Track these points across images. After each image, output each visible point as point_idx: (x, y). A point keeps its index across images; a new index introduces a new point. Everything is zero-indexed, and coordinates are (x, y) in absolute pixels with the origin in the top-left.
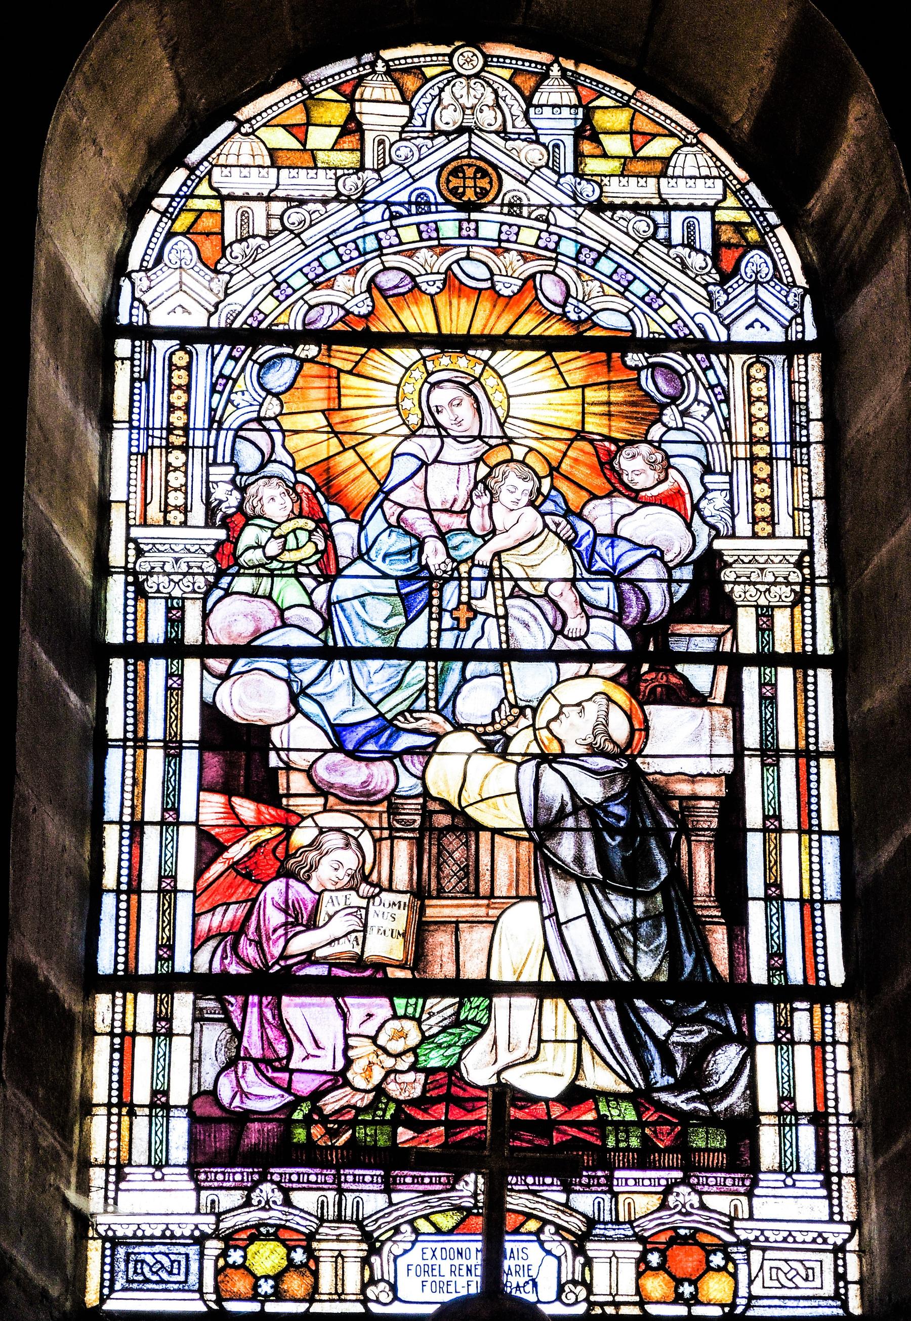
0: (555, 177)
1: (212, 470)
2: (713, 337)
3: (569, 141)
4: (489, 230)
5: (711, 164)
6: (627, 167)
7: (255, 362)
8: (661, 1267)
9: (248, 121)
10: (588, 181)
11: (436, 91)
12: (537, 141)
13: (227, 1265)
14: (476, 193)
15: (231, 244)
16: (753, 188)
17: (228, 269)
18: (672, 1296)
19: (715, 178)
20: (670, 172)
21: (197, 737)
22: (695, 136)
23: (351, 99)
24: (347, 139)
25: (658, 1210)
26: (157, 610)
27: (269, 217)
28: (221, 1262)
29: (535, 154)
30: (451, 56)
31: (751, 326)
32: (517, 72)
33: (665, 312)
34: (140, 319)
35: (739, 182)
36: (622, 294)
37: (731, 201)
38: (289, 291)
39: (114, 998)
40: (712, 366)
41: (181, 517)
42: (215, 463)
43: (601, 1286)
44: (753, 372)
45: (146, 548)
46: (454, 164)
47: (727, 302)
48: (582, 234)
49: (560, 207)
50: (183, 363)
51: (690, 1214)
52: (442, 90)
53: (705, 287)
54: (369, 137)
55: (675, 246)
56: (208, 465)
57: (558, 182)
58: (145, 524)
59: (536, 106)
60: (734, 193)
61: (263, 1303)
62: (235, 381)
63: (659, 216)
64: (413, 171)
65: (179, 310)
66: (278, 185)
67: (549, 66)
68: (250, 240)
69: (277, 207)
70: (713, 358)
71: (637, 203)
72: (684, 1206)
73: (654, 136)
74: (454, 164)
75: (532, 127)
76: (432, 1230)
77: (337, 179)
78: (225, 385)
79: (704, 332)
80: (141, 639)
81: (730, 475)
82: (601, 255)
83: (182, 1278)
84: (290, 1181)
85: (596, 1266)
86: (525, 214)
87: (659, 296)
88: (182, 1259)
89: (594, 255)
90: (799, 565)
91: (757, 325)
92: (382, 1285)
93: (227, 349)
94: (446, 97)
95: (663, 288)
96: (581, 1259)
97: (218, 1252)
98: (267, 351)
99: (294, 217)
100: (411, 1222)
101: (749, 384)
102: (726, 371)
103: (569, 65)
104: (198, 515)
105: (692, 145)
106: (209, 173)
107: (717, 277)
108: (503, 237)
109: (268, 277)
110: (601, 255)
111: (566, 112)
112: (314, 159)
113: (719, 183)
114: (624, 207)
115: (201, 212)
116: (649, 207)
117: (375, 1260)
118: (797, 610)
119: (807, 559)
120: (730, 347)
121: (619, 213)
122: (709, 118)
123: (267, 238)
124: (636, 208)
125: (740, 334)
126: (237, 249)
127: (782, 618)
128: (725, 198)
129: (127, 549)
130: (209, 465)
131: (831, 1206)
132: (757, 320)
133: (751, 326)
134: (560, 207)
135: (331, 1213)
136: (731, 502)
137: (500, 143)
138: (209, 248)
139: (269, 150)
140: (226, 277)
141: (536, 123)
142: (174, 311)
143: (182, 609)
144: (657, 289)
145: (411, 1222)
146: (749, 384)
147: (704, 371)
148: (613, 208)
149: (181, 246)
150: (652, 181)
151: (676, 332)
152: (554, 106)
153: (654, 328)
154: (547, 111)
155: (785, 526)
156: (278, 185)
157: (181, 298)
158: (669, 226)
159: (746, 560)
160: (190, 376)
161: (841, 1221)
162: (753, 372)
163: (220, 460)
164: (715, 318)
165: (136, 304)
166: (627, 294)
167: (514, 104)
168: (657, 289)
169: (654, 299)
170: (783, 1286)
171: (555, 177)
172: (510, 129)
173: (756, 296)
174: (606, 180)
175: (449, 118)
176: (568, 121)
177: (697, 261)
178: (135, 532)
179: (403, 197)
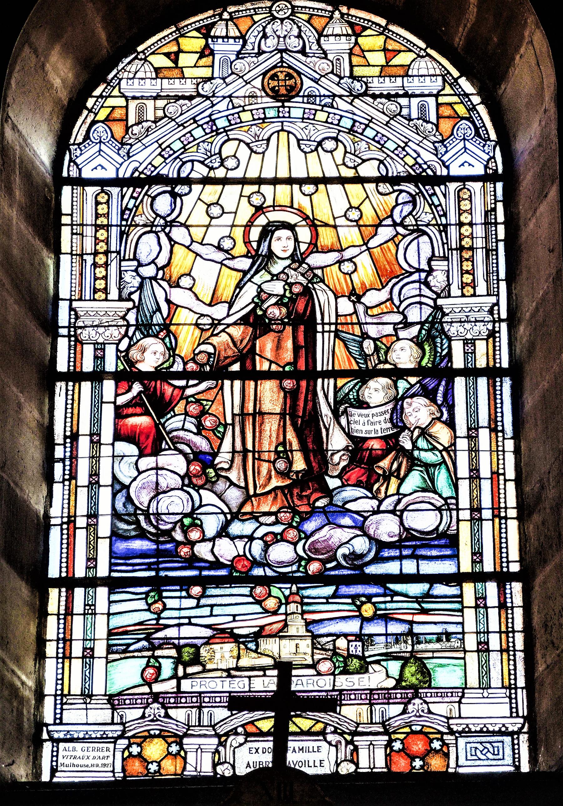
0: (337, 79)
1: (123, 263)
3: (346, 57)
4: (297, 113)
5: (436, 66)
6: (385, 71)
7: (149, 196)
9: (143, 52)
10: (358, 81)
11: (261, 28)
12: (326, 58)
14: (286, 90)
15: (132, 126)
16: (463, 82)
17: (129, 142)
20: (410, 73)
21: (56, 464)
22: (425, 50)
23: (206, 36)
24: (204, 60)
26: (88, 350)
27: (155, 109)
28: (126, 754)
29: (324, 66)
30: (270, 8)
34: (74, 173)
35: (453, 78)
37: (448, 90)
38: (171, 152)
39: (60, 592)
40: (435, 194)
42: (124, 260)
43: (364, 763)
45: (82, 314)
46: (272, 72)
47: (446, 152)
48: (354, 114)
49: (340, 97)
50: (104, 200)
52: (264, 28)
53: (434, 143)
54: (217, 57)
55: (413, 120)
57: (339, 82)
60: (450, 85)
63: (404, 101)
64: (246, 78)
65: (99, 168)
67: (333, 12)
68: (144, 124)
69: (161, 103)
70: (436, 188)
71: (389, 94)
72: (418, 711)
73: (400, 51)
74: (272, 72)
75: (322, 49)
80: (78, 370)
84: (170, 703)
86: (318, 102)
87: (403, 149)
89: (363, 126)
90: (491, 312)
91: (466, 164)
92: (226, 765)
95: (406, 144)
97: (124, 746)
99: (172, 109)
101: (459, 202)
103: (344, 9)
104: (114, 294)
105: (423, 57)
109: (156, 145)
110: (367, 126)
112: (182, 72)
113: (440, 79)
114: (381, 96)
115: (114, 108)
116: (397, 95)
118: (491, 340)
119: (496, 308)
121: (378, 100)
122: (437, 40)
123: (155, 122)
124: (388, 97)
125: (455, 171)
126: (136, 129)
127: (481, 346)
128: (443, 89)
129: (70, 315)
131: (511, 708)
134: (340, 97)
136: (448, 277)
137: (303, 58)
138: (119, 130)
139: (154, 68)
141: (325, 47)
142: (96, 168)
143: (104, 350)
144: (403, 145)
146: (459, 202)
147: (430, 196)
148: (374, 97)
149: (101, 129)
150: (399, 80)
151: (414, 171)
152: (336, 35)
153: (401, 169)
155: (482, 288)
157: (100, 160)
158: (409, 107)
161: (518, 716)
163: (127, 257)
167: (310, 35)
168: (403, 145)
170: (480, 759)
172: (308, 50)
173: (465, 147)
174: (370, 80)
176: (344, 44)
178: (75, 304)
179: (241, 93)
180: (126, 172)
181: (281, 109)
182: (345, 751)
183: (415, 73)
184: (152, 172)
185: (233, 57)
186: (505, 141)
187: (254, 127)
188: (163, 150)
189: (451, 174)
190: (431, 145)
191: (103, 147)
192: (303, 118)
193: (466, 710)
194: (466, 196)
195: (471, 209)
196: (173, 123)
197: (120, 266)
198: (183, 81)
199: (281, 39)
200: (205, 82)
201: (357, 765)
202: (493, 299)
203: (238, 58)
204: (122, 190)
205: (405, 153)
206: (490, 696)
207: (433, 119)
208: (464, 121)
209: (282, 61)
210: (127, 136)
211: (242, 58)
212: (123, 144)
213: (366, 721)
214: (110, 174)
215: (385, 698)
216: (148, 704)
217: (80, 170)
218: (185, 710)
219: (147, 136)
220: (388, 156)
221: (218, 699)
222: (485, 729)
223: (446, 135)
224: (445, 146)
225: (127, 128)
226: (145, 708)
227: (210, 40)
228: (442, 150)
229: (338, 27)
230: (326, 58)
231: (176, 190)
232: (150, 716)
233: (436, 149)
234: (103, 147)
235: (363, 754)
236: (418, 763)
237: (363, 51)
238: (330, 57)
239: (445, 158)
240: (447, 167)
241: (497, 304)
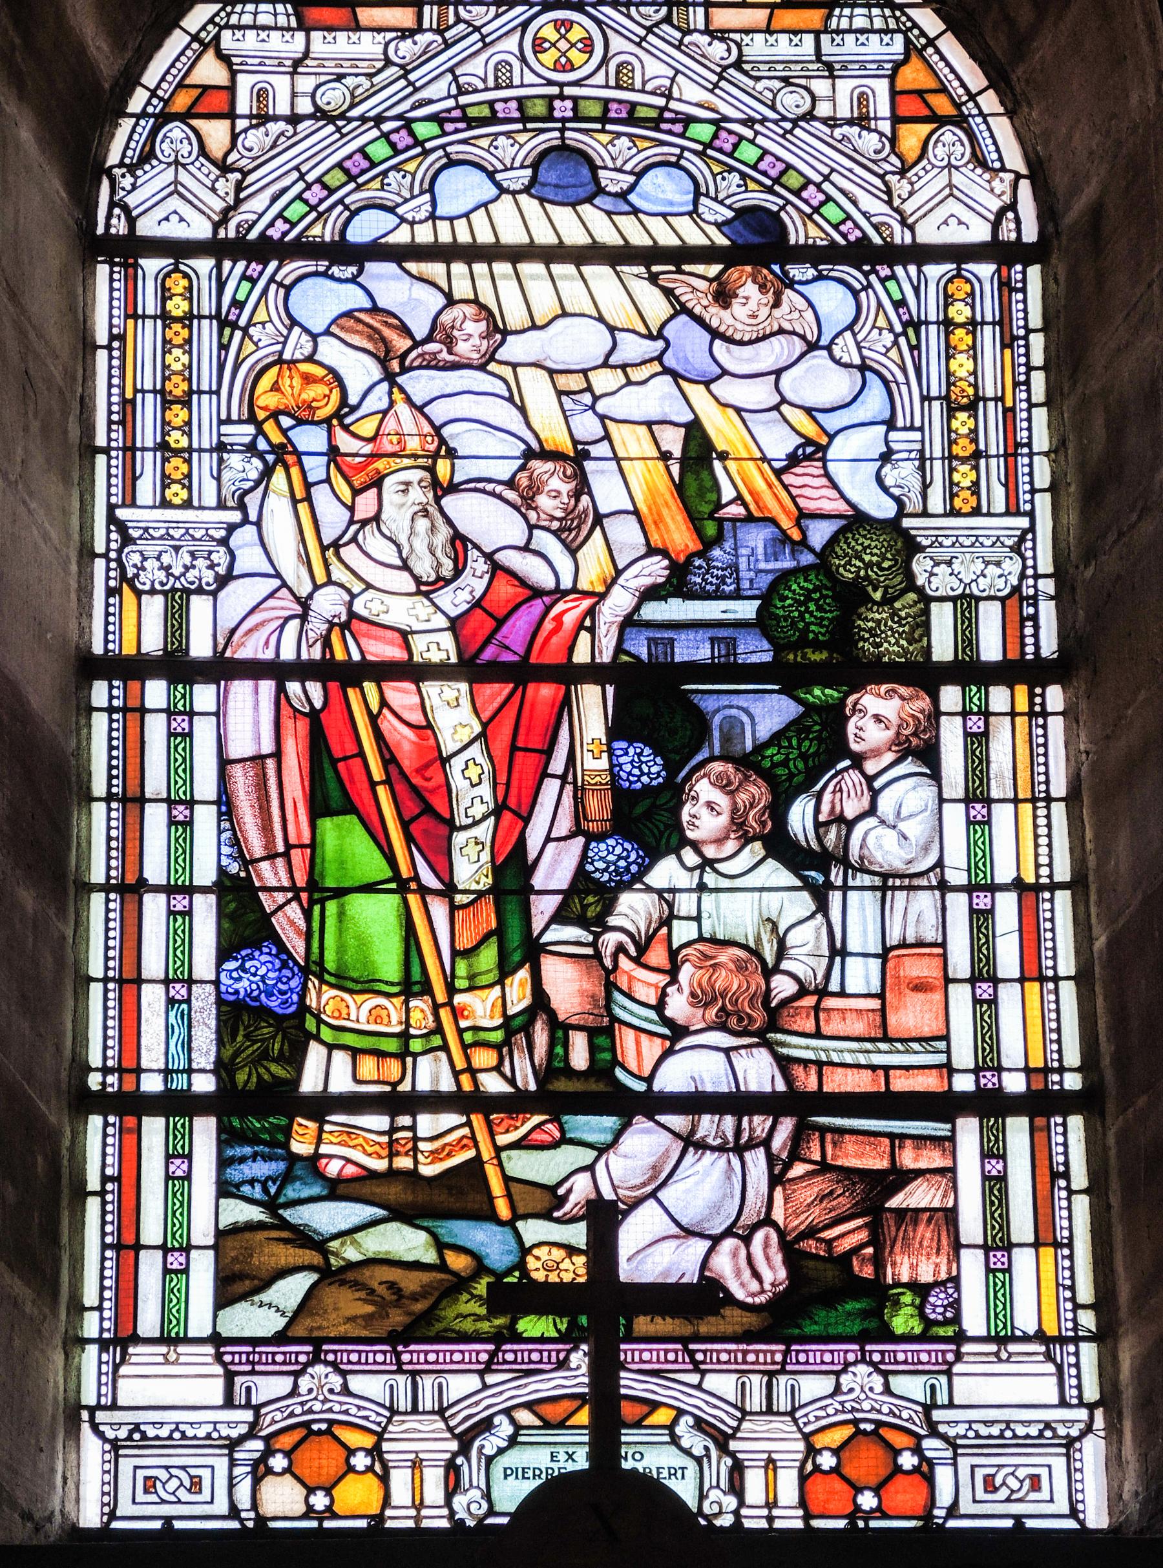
1: (225, 429)
10: (722, 40)
19: (893, 31)
25: (832, 1396)
34: (120, 227)
47: (134, 187)
53: (882, 177)
56: (221, 422)
57: (681, 41)
61: (321, 1520)
70: (899, 270)
76: (538, 1423)
77: (387, 45)
81: (921, 429)
93: (241, 266)
95: (826, 178)
98: (293, 268)
100: (507, 1412)
102: (916, 290)
106: (217, 37)
107: (898, 164)
113: (899, 39)
135: (756, 1400)
140: (238, 176)
142: (167, 219)
145: (507, 1412)
151: (844, 236)
157: (952, 206)
159: (967, 542)
163: (235, 417)
165: (117, 211)
171: (678, 35)
174: (747, 39)
177: (869, 142)
178: (121, 514)
188: (818, 186)
193: (965, 1390)
198: (354, 37)
200: (403, 38)
204: (219, 266)
205: (821, 197)
206: (182, 1359)
213: (756, 1408)
214: (201, 229)
215: (248, 1362)
216: (847, 1365)
218: (925, 1378)
220: (788, 202)
223: (912, 156)
226: (297, 1375)
228: (901, 187)
232: (310, 1391)
234: (183, 176)
239: (908, 207)
240: (911, 228)
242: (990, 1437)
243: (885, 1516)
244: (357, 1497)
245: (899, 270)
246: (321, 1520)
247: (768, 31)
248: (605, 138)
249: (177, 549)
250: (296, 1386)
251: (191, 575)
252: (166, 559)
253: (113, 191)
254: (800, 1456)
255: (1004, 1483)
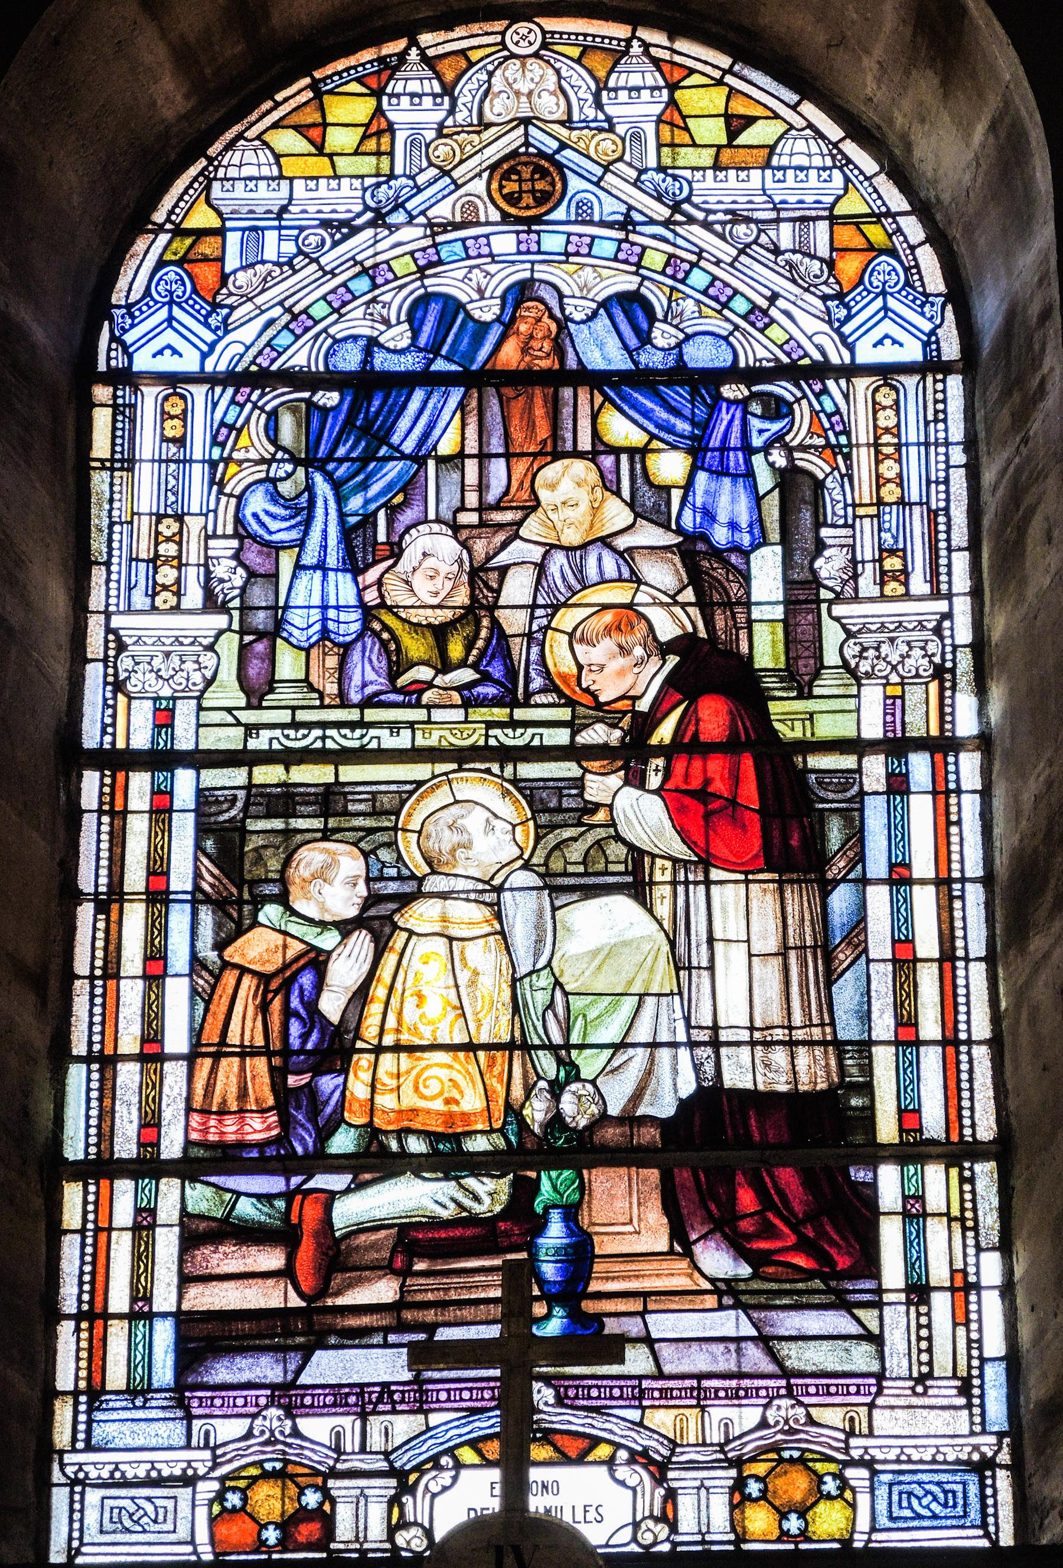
1: (212, 543)
2: (835, 360)
8: (764, 1496)
13: (224, 1509)
15: (235, 272)
17: (228, 301)
18: (776, 1533)
20: (775, 161)
28: (216, 1509)
30: (503, 34)
31: (880, 342)
32: (586, 49)
33: (774, 332)
34: (119, 361)
36: (719, 312)
41: (173, 601)
42: (215, 536)
43: (687, 1522)
44: (879, 397)
51: (798, 1431)
52: (491, 74)
54: (401, 137)
55: (783, 253)
56: (207, 537)
57: (638, 179)
58: (129, 611)
59: (610, 90)
61: (796, 1543)
62: (240, 431)
65: (168, 352)
66: (291, 199)
67: (628, 41)
68: (258, 267)
72: (786, 1422)
78: (228, 437)
79: (823, 353)
82: (693, 265)
83: (169, 1526)
85: (681, 1499)
88: (959, 1488)
92: (414, 1531)
93: (230, 391)
94: (497, 82)
96: (661, 1491)
97: (212, 1495)
102: (846, 396)
104: (194, 597)
108: (571, 249)
110: (693, 265)
111: (645, 94)
117: (407, 1499)
120: (851, 371)
125: (866, 354)
126: (242, 278)
130: (207, 537)
132: (887, 336)
133: (880, 342)
140: (225, 311)
141: (610, 110)
150: (756, 174)
152: (631, 89)
153: (762, 353)
154: (623, 95)
156: (291, 199)
157: (169, 337)
160: (185, 426)
162: (879, 397)
163: (219, 532)
164: (219, 347)
166: (726, 312)
169: (759, 316)
174: (698, 175)
175: (498, 109)
176: (651, 106)
178: (116, 622)
180: (219, 363)
181: (523, 237)
182: (652, 1497)
183: (785, 161)
184: (273, 361)
185: (430, 135)
186: (959, 296)
187: (476, 271)
189: (859, 360)
190: (819, 303)
191: (177, 312)
192: (567, 254)
194: (887, 402)
195: (898, 425)
196: (314, 266)
197: (206, 548)
199: (524, 99)
201: (674, 1528)
202: (942, 606)
203: (440, 135)
207: (823, 251)
208: (883, 258)
209: (527, 144)
210: (224, 291)
211: (447, 136)
212: (215, 306)
214: (189, 363)
217: (130, 357)
218: (675, 1412)
219: (263, 291)
221: (466, 1395)
222: (904, 1458)
224: (847, 306)
225: (224, 278)
227: (385, 99)
229: (637, 73)
230: (611, 129)
231: (315, 399)
233: (828, 312)
234: (177, 312)
235: (686, 1505)
236: (793, 1524)
237: (684, 118)
238: (620, 129)
240: (851, 348)
241: (948, 616)
242: (921, 1462)
243: (809, 1540)
244: (829, 1521)
245: (831, 384)
246: (796, 1543)
247: (717, 167)
248: (571, 268)
249: (892, 640)
250: (251, 1428)
251: (179, 678)
252: (156, 663)
253: (112, 331)
254: (393, 1492)
255: (927, 1507)
